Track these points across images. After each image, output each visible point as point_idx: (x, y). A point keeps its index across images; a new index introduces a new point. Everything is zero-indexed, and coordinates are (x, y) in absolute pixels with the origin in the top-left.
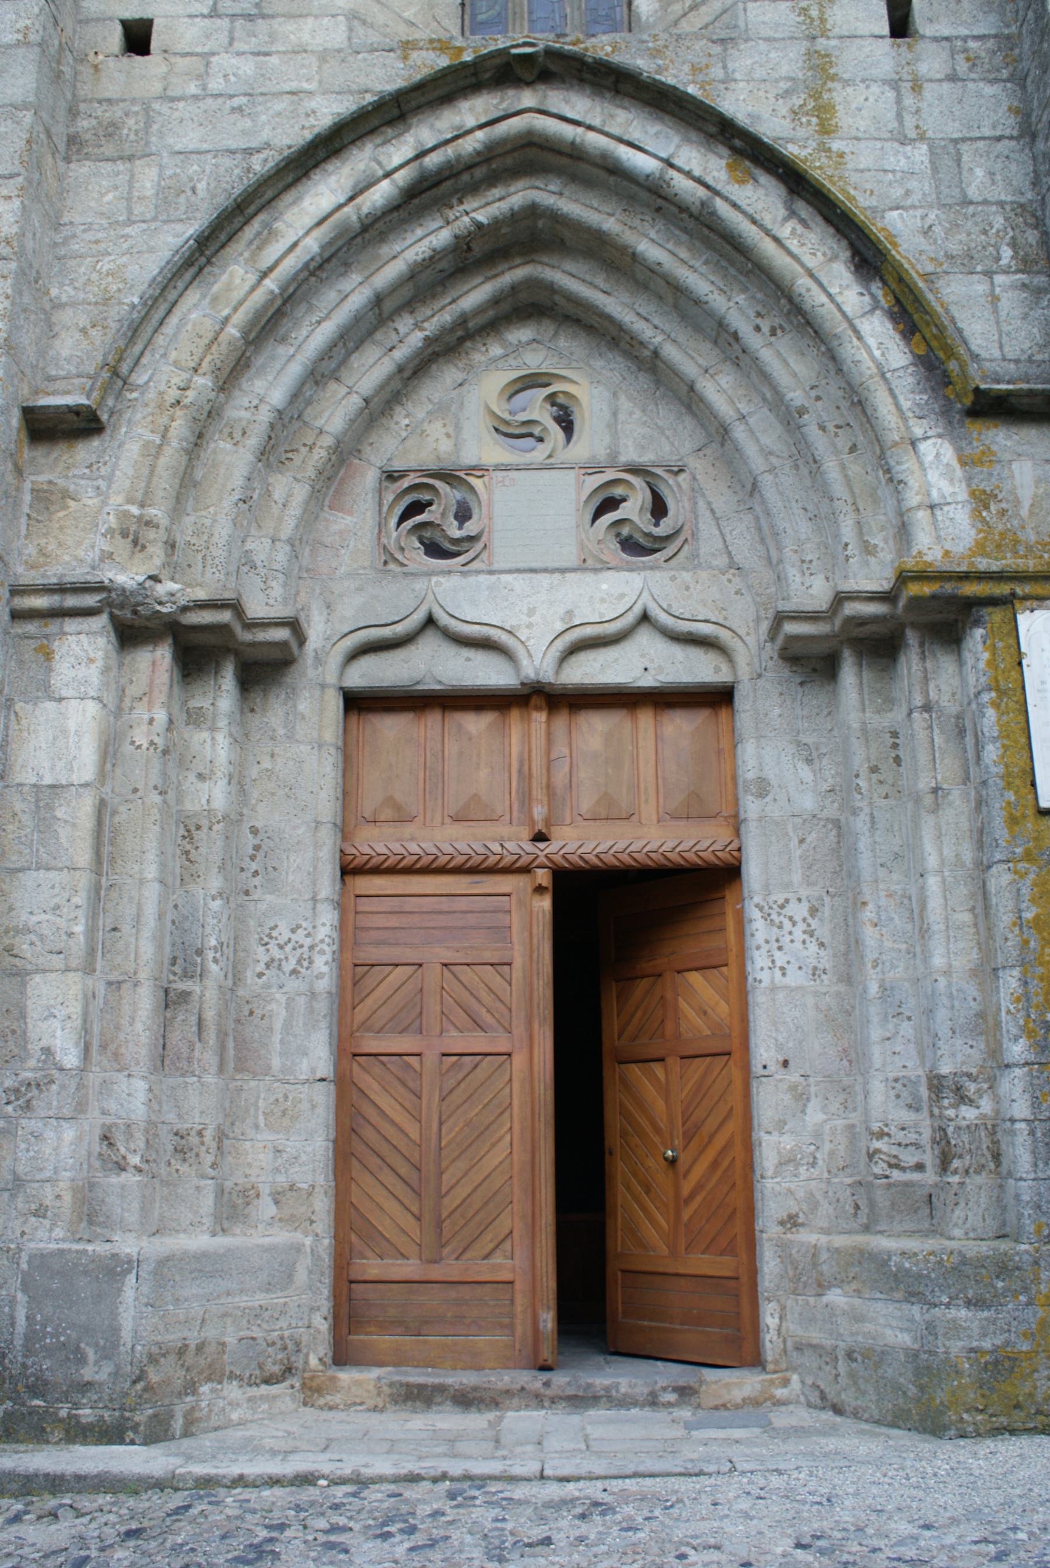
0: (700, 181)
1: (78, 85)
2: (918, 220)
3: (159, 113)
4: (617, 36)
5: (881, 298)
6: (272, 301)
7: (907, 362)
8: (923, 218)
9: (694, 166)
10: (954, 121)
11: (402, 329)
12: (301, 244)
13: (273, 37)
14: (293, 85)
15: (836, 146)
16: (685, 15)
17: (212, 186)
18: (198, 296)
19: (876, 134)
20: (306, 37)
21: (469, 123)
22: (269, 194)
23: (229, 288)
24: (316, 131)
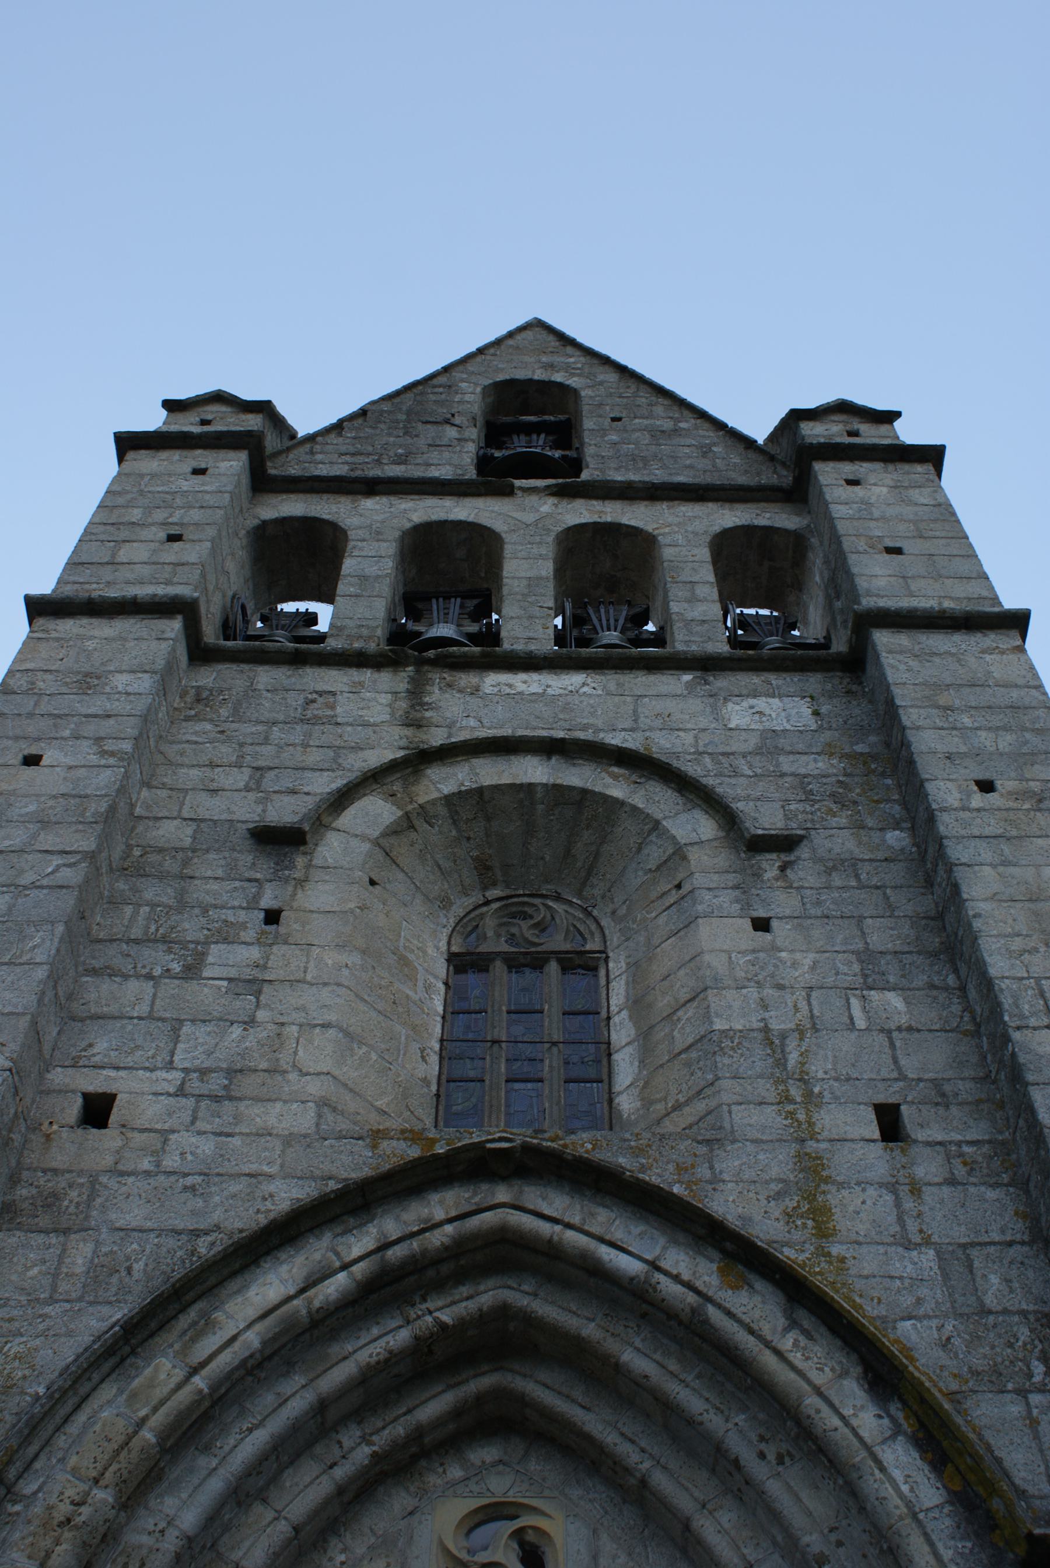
0: (689, 1286)
1: (26, 1152)
2: (935, 1332)
3: (106, 1187)
4: (598, 1135)
5: (902, 1421)
6: (198, 1403)
7: (941, 1500)
8: (940, 1328)
9: (683, 1270)
10: (959, 1225)
11: (347, 1443)
12: (241, 1338)
13: (237, 1118)
14: (253, 1168)
15: (836, 1250)
16: (668, 1114)
17: (151, 1267)
18: (114, 1391)
19: (877, 1238)
20: (272, 1121)
21: (439, 1215)
22: (213, 1280)
23: (151, 1384)
24: (272, 1216)
